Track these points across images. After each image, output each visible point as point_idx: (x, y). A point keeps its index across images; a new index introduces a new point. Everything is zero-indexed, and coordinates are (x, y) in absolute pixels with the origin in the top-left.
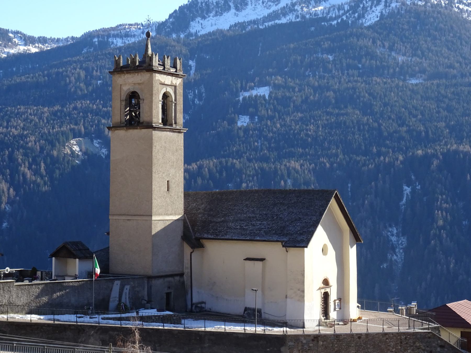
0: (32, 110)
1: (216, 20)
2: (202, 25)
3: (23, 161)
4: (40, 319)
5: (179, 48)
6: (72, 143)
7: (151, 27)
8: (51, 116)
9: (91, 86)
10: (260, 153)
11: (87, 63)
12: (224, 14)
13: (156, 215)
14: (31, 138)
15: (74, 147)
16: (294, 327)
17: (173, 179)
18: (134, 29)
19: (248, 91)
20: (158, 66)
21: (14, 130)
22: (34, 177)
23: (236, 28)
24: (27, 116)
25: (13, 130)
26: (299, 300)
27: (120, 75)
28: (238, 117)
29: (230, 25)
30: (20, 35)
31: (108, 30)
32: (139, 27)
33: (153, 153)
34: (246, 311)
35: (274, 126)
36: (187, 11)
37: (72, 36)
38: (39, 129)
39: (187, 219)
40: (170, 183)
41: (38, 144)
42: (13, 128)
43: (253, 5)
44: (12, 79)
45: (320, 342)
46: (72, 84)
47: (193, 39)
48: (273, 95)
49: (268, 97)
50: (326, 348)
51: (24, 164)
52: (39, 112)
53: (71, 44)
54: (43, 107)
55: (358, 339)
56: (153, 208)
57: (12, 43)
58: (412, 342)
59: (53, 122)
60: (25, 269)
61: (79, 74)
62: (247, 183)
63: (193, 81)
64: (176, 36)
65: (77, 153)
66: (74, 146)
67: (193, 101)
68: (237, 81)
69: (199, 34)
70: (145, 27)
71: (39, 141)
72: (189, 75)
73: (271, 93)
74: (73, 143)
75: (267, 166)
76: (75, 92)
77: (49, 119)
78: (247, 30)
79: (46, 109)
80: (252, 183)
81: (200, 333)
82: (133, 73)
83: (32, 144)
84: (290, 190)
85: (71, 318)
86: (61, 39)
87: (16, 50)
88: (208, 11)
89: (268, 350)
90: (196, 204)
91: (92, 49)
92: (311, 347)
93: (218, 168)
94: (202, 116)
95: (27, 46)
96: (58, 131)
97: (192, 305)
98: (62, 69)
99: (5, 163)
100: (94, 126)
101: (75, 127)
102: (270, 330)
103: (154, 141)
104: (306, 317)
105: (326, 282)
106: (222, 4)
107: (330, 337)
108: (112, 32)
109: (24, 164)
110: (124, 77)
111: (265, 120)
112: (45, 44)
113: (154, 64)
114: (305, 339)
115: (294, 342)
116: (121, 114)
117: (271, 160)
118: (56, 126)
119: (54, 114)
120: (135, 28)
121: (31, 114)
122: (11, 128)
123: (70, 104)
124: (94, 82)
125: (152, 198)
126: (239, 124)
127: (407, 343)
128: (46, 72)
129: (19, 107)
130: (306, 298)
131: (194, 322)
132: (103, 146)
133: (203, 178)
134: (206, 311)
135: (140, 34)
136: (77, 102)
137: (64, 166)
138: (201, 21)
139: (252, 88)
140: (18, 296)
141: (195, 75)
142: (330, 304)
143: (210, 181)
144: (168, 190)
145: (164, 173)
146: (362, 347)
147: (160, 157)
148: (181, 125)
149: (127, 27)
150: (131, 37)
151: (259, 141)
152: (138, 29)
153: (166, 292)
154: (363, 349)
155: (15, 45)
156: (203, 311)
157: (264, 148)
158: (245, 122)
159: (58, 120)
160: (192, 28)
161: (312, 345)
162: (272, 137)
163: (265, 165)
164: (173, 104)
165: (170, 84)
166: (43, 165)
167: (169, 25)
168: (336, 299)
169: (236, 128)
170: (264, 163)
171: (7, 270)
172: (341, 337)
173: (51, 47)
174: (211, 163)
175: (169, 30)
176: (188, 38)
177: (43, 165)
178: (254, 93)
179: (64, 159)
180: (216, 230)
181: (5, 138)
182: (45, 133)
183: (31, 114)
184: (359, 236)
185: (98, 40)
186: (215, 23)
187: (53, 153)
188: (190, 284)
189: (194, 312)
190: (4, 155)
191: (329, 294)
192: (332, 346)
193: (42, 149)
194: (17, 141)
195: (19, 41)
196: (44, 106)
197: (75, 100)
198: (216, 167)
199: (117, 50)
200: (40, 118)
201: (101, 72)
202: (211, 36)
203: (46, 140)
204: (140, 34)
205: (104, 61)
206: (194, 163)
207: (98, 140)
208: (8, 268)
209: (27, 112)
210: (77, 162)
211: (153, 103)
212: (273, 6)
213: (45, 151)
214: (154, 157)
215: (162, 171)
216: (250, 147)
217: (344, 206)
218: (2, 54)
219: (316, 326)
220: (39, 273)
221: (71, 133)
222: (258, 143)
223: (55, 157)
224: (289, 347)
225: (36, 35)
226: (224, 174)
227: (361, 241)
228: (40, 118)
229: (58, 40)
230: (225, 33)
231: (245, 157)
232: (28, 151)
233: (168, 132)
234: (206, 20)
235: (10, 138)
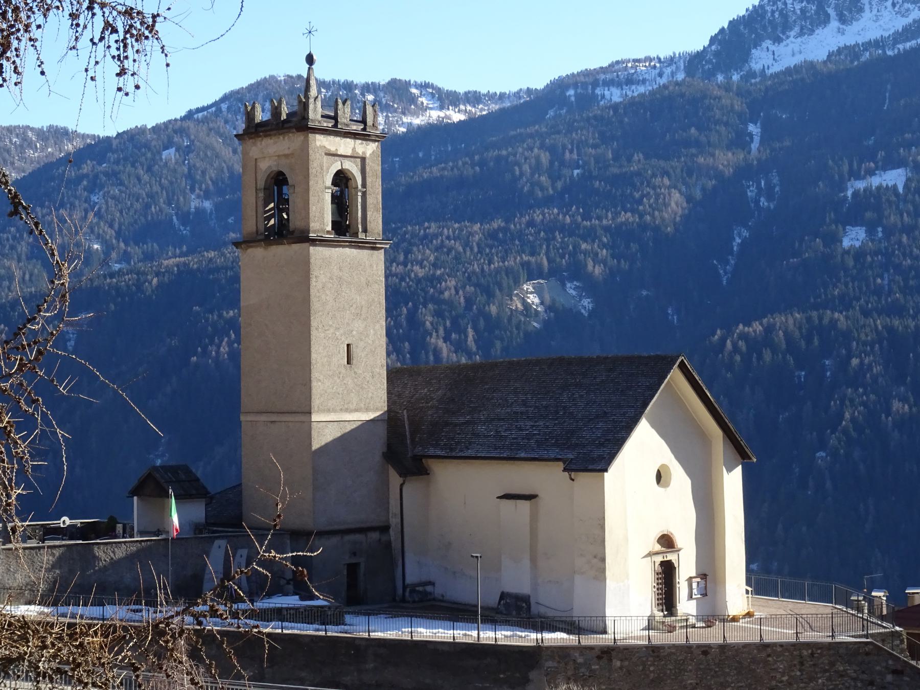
0: (451, 230)
1: (801, 44)
2: (774, 54)
3: (435, 326)
4: (42, 613)
5: (728, 102)
6: (525, 289)
7: (675, 63)
8: (485, 238)
9: (560, 180)
10: (886, 300)
11: (553, 136)
12: (817, 32)
13: (320, 411)
14: (448, 282)
15: (529, 298)
16: (587, 630)
17: (361, 340)
18: (644, 68)
19: (864, 178)
20: (320, 119)
21: (418, 267)
22: (454, 355)
23: (841, 57)
24: (442, 241)
25: (417, 268)
26: (595, 578)
27: (254, 141)
28: (844, 229)
29: (829, 53)
30: (430, 91)
31: (595, 73)
32: (652, 64)
33: (312, 291)
34: (503, 599)
35: (914, 245)
36: (745, 28)
37: (528, 88)
38: (464, 266)
39: (406, 420)
40: (353, 349)
41: (461, 292)
42: (417, 264)
43: (875, 11)
44: (415, 173)
45: (614, 661)
46: (524, 178)
47: (756, 84)
48: (913, 185)
49: (904, 188)
50: (629, 672)
51: (437, 332)
52: (465, 232)
53: (526, 102)
54: (471, 223)
55: (701, 656)
56: (313, 397)
57: (416, 105)
58: (826, 661)
59: (491, 252)
60: (102, 520)
61: (538, 158)
62: (860, 357)
63: (755, 162)
64: (724, 78)
65: (535, 307)
66: (528, 295)
67: (757, 202)
68: (842, 160)
69: (769, 72)
70: (665, 64)
71: (464, 287)
72: (749, 152)
73: (908, 179)
74: (527, 289)
75: (901, 323)
76: (531, 192)
77: (483, 245)
78: (863, 59)
79: (477, 227)
80: (872, 358)
81: (357, 642)
82: (275, 135)
83: (451, 294)
84: (598, 357)
85: (701, 632)
86: (508, 93)
87: (424, 118)
88: (786, 27)
89: (502, 676)
90: (429, 390)
91: (564, 111)
92: (595, 671)
93: (804, 331)
94: (774, 231)
95: (444, 111)
96: (499, 267)
97: (405, 587)
98: (507, 149)
99: (401, 331)
100: (567, 256)
101: (531, 258)
102: (521, 637)
103: (313, 267)
104: (610, 612)
105: (667, 541)
106: (813, 12)
107: (638, 652)
108: (602, 77)
109: (437, 332)
110: (261, 144)
111: (897, 234)
112: (478, 105)
113: (311, 115)
114: (582, 654)
115: (559, 662)
116: (257, 217)
117: (909, 311)
118: (495, 257)
119: (493, 235)
120: (645, 66)
121: (448, 238)
122: (412, 265)
123: (522, 215)
124: (566, 171)
125: (310, 378)
126: (846, 243)
127: (814, 665)
128: (477, 157)
129: (426, 224)
130: (608, 574)
131: (385, 620)
132: (584, 294)
133: (774, 351)
134: (434, 599)
135: (655, 78)
136: (534, 212)
137: (511, 332)
138: (772, 48)
139: (871, 173)
140: (10, 570)
141: (759, 151)
142: (678, 585)
143: (788, 356)
144: (349, 362)
145: (337, 329)
146: (712, 673)
147: (328, 298)
148: (379, 234)
149: (630, 65)
150: (638, 84)
151: (886, 275)
152: (652, 68)
153: (348, 562)
154: (713, 676)
155: (421, 109)
156: (430, 600)
157: (895, 288)
158: (858, 240)
159: (498, 248)
160: (754, 62)
161: (597, 667)
162: (911, 268)
163: (896, 322)
164: (360, 194)
165: (349, 155)
166: (471, 333)
167: (709, 58)
168: (694, 575)
169: (840, 250)
170: (894, 317)
171: (64, 521)
172: (661, 651)
173: (488, 109)
174: (791, 321)
175: (710, 66)
176: (747, 81)
177: (471, 333)
178: (875, 181)
179: (510, 319)
180: (453, 439)
181: (400, 284)
182: (474, 272)
183: (448, 238)
184: (745, 447)
185: (576, 92)
186: (800, 50)
187: (490, 311)
188: (400, 545)
189: (409, 602)
190: (400, 315)
191: (676, 565)
192: (642, 670)
193: (469, 302)
194: (422, 290)
195: (429, 102)
196: (472, 220)
197: (531, 207)
198: (800, 328)
199: (609, 109)
200: (467, 244)
201: (578, 155)
202: (791, 75)
203: (477, 285)
204: (655, 78)
205: (585, 132)
206: (757, 323)
207: (575, 283)
208: (65, 518)
209: (441, 234)
210: (535, 324)
211: (311, 193)
212: (913, 10)
213: (475, 307)
214: (313, 299)
215: (334, 325)
216: (868, 286)
217: (704, 388)
218: (398, 128)
219: (643, 630)
220: (119, 527)
221: (524, 273)
222: (882, 279)
223: (493, 316)
224: (547, 670)
225: (461, 89)
226: (816, 342)
227: (750, 458)
228: (467, 244)
229: (502, 96)
230: (818, 67)
231: (858, 308)
232: (444, 307)
233: (347, 249)
234: (782, 45)
235: (411, 283)
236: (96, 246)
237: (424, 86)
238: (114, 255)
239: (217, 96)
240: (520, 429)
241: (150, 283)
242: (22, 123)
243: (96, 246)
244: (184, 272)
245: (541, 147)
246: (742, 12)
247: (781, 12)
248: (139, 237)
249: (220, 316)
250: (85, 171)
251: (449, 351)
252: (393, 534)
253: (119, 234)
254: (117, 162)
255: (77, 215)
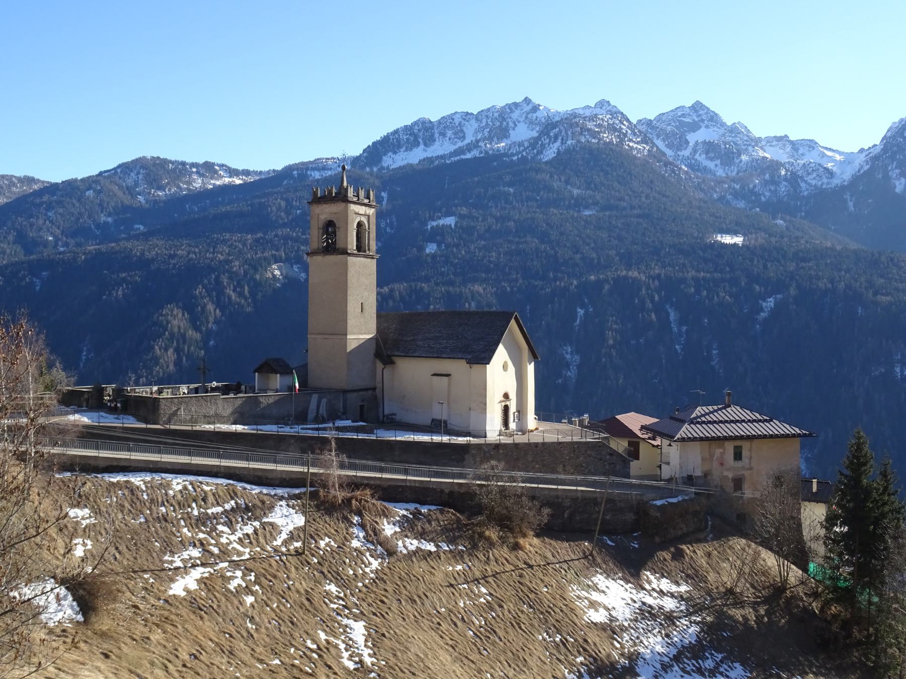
4: (244, 429)
25: (219, 255)
61: (280, 204)
67: (385, 229)
69: (391, 168)
73: (456, 222)
78: (435, 164)
88: (399, 146)
97: (384, 416)
104: (488, 428)
105: (506, 396)
108: (311, 166)
113: (349, 195)
119: (257, 241)
121: (235, 241)
123: (272, 232)
126: (428, 251)
138: (392, 156)
139: (440, 218)
163: (451, 289)
166: (246, 288)
177: (246, 288)
178: (441, 222)
179: (266, 282)
183: (235, 241)
193: (246, 273)
196: (247, 233)
200: (244, 245)
208: (214, 382)
209: (232, 239)
214: (349, 281)
220: (243, 387)
225: (240, 168)
228: (244, 245)
229: (261, 172)
236: (50, 238)
237: (221, 166)
238: (60, 243)
239: (115, 165)
240: (440, 344)
241: (81, 258)
242: (10, 173)
243: (50, 238)
244: (99, 253)
245: (282, 198)
246: (379, 139)
247: (397, 140)
248: (74, 235)
249: (118, 276)
250: (45, 200)
251: (236, 297)
252: (378, 391)
253: (63, 232)
254: (62, 196)
255: (41, 222)
